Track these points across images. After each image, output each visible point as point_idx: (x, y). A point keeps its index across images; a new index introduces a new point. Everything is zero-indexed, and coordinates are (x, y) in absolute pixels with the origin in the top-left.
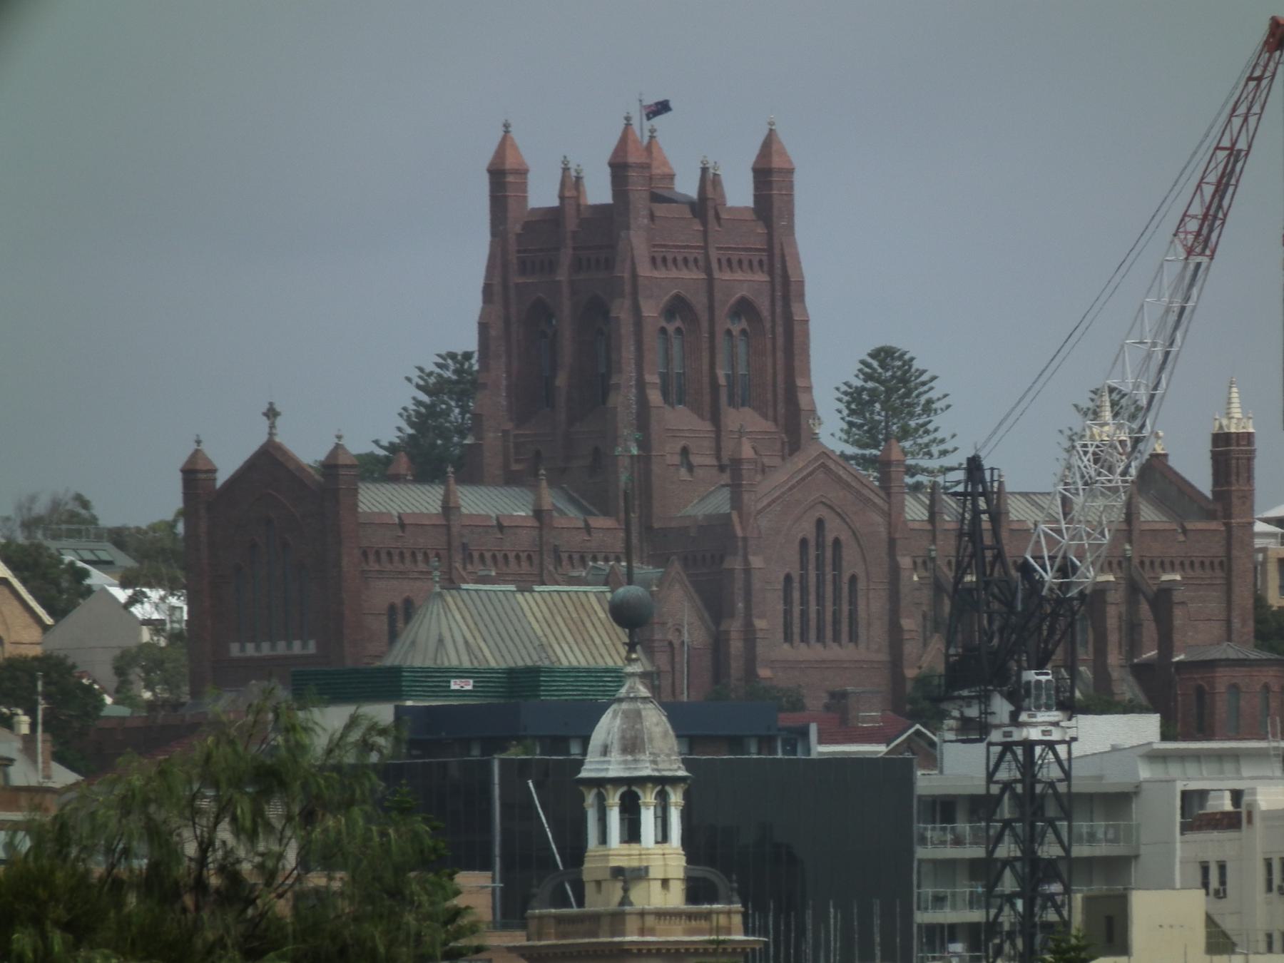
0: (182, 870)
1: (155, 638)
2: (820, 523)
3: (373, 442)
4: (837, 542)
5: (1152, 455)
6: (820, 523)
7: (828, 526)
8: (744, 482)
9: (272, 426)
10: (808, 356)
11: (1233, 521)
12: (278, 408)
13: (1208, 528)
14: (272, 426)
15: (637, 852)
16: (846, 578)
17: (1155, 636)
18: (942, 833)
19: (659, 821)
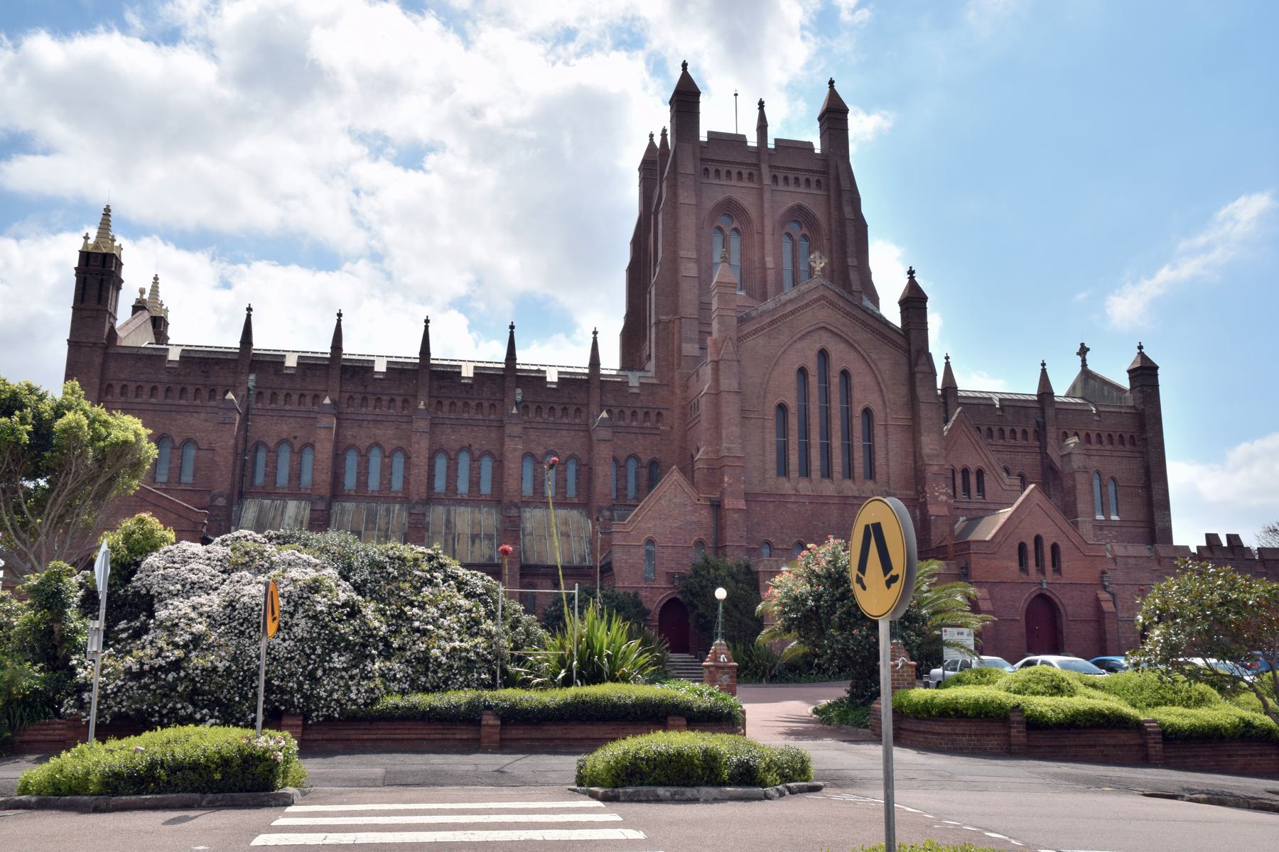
0: (113, 24)
1: (393, 151)
2: (823, 354)
3: (1082, 345)
4: (867, 412)
5: (824, 276)
6: (823, 354)
7: (834, 355)
8: (1150, 435)
9: (1084, 361)
10: (698, 113)
11: (559, 561)
12: (1087, 345)
13: (1034, 555)
14: (1084, 361)
15: (528, 468)
16: (857, 410)
17: (522, 839)
18: (316, 444)
19: (891, 827)
